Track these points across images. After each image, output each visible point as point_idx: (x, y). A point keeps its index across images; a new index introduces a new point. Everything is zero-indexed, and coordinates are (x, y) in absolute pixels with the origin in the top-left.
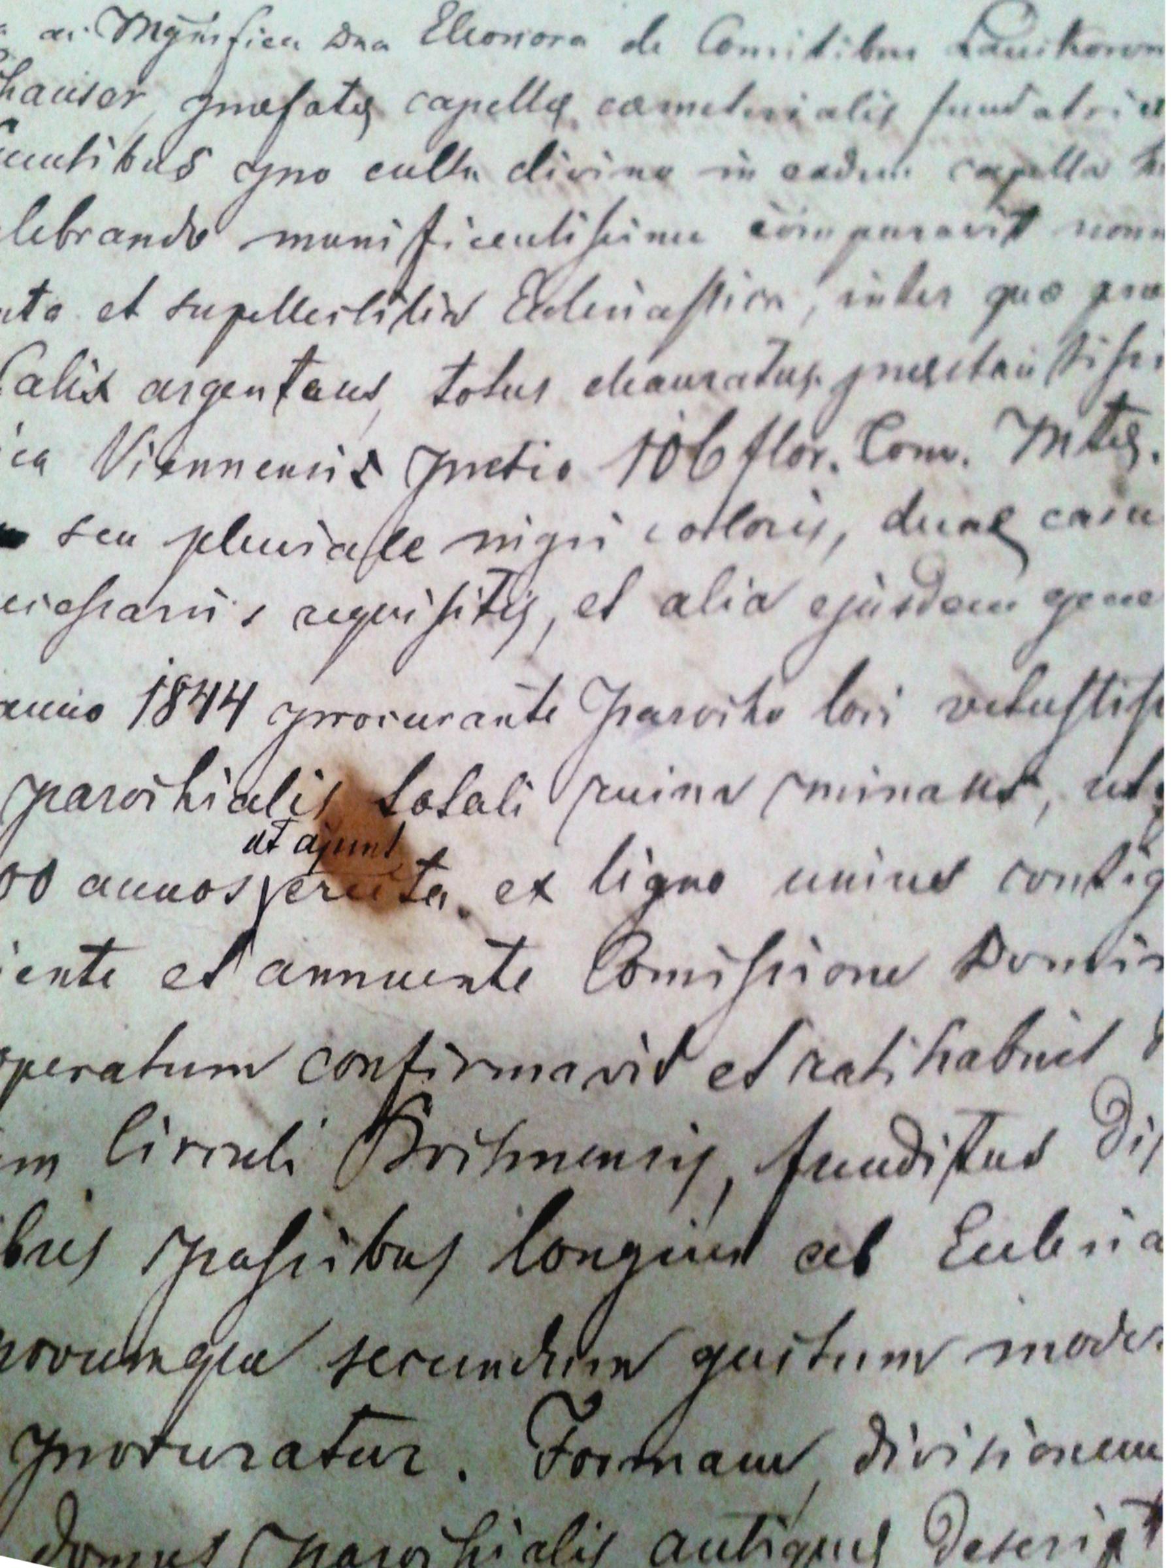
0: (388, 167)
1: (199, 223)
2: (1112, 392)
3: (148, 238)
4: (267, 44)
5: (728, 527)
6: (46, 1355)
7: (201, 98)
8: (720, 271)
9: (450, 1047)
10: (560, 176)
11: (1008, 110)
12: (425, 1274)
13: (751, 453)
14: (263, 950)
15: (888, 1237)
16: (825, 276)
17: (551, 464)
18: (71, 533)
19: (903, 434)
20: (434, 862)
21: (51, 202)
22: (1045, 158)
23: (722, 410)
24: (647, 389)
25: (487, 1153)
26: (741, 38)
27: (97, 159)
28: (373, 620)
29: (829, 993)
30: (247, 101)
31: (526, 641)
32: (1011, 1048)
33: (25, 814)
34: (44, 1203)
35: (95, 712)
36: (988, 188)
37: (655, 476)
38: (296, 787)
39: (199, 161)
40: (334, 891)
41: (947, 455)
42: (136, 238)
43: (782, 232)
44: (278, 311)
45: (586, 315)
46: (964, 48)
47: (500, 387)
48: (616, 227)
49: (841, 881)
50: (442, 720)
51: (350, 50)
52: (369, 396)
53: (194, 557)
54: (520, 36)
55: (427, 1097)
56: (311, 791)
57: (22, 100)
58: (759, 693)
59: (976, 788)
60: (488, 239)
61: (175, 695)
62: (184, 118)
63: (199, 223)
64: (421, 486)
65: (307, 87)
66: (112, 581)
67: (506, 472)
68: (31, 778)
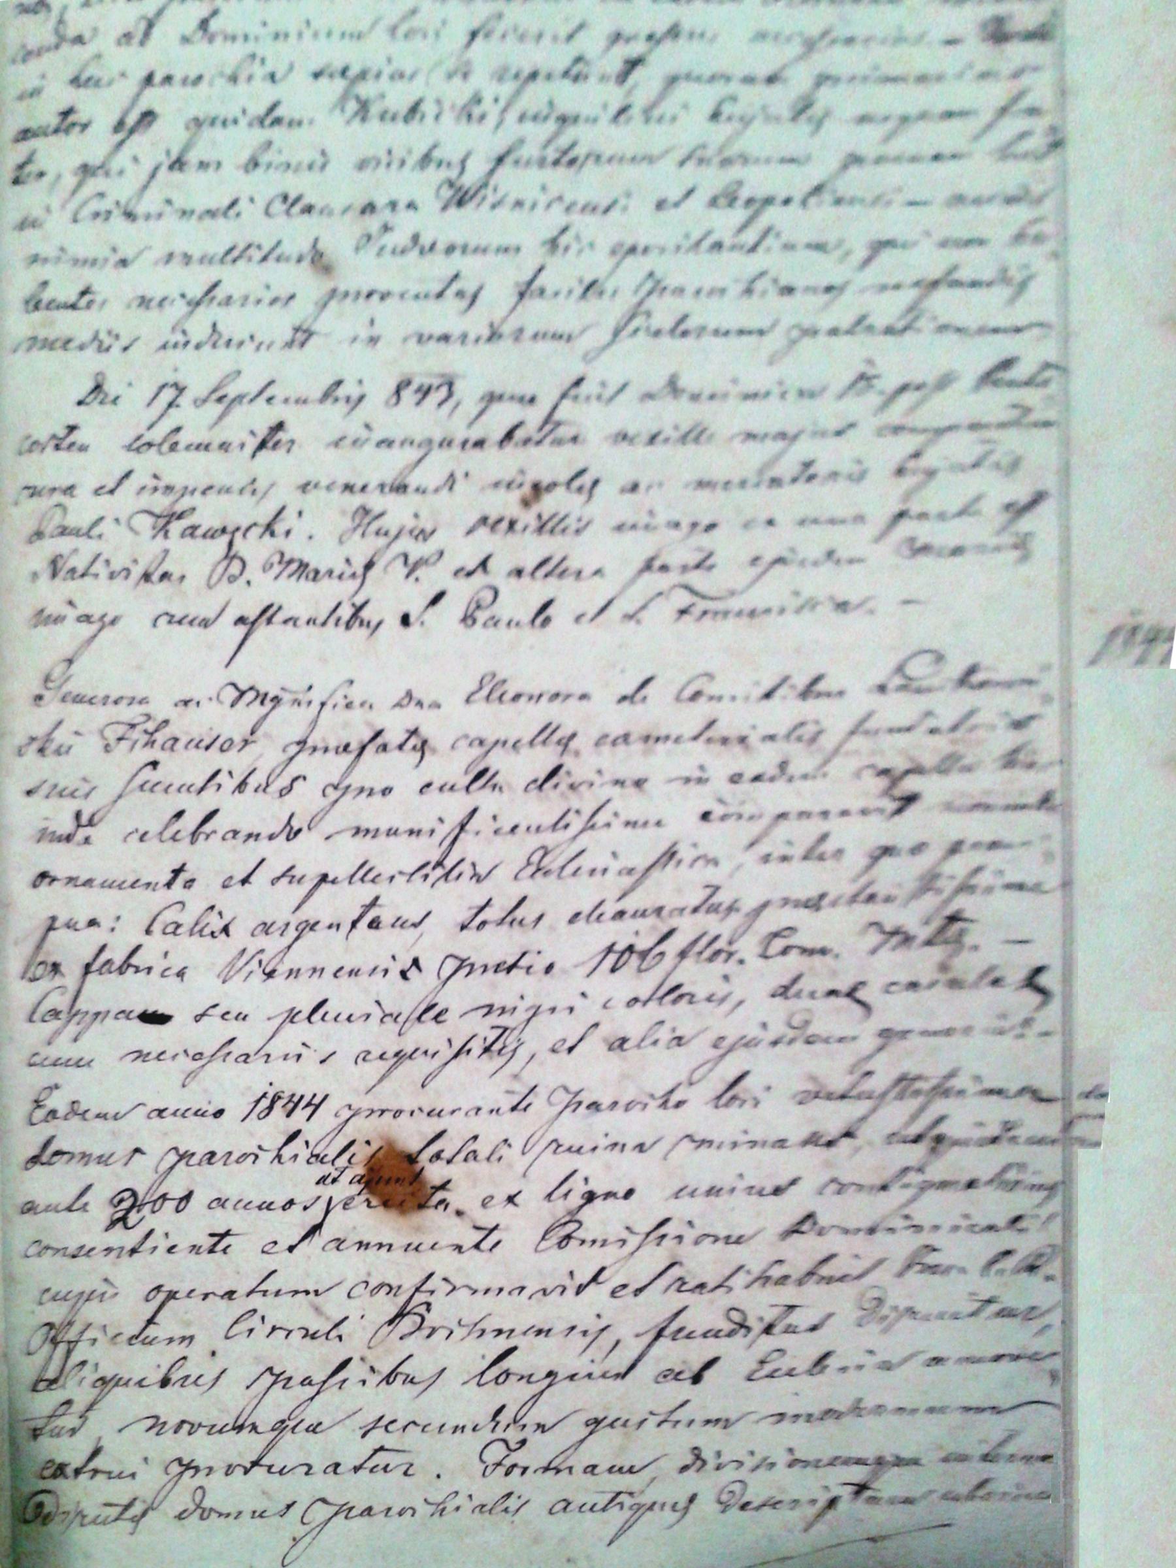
0: (436, 785)
1: (296, 824)
2: (949, 911)
3: (258, 835)
4: (348, 706)
5: (662, 998)
6: (186, 1427)
7: (298, 743)
8: (675, 844)
9: (445, 1279)
10: (563, 787)
11: (909, 729)
12: (420, 1387)
13: (683, 954)
14: (328, 1232)
15: (716, 1367)
16: (752, 844)
17: (540, 964)
18: (203, 1015)
19: (794, 940)
20: (443, 1187)
21: (186, 815)
22: (928, 760)
23: (665, 930)
24: (613, 918)
25: (465, 1331)
26: (712, 689)
27: (219, 786)
28: (410, 1057)
29: (697, 1249)
30: (332, 744)
31: (514, 1066)
32: (811, 1273)
33: (172, 1168)
34: (184, 1358)
35: (219, 1113)
36: (883, 782)
37: (613, 970)
38: (352, 1149)
39: (296, 785)
40: (374, 1202)
41: (823, 951)
42: (250, 836)
43: (723, 818)
44: (352, 876)
45: (575, 873)
46: (882, 688)
47: (509, 919)
48: (600, 819)
49: (713, 1191)
50: (453, 1112)
51: (412, 709)
52: (415, 925)
53: (288, 1026)
54: (540, 696)
55: (428, 1305)
56: (362, 1153)
57: (163, 748)
58: (672, 1091)
59: (812, 1140)
60: (507, 828)
61: (273, 1102)
62: (284, 757)
63: (296, 824)
64: (449, 978)
65: (378, 734)
66: (232, 1040)
67: (509, 970)
68: (176, 1149)
